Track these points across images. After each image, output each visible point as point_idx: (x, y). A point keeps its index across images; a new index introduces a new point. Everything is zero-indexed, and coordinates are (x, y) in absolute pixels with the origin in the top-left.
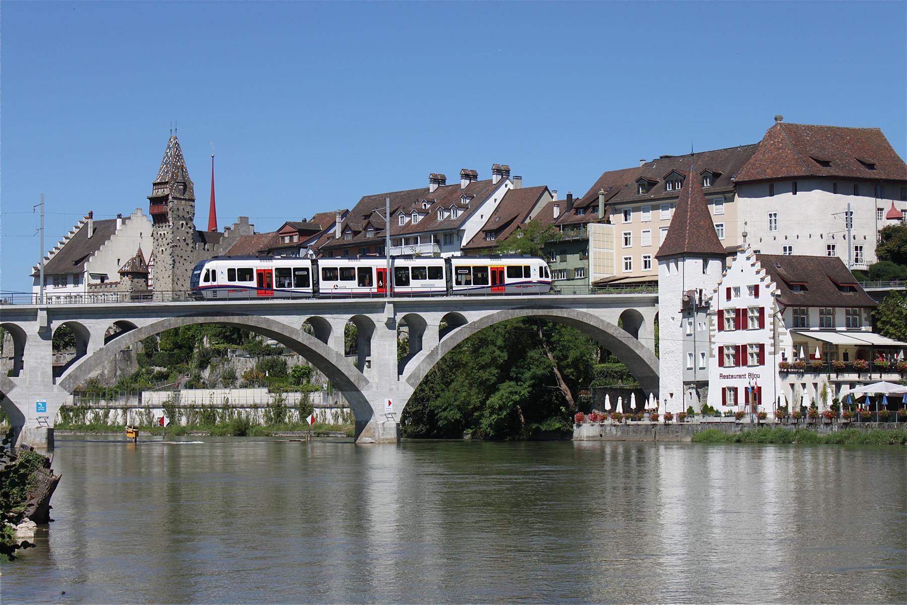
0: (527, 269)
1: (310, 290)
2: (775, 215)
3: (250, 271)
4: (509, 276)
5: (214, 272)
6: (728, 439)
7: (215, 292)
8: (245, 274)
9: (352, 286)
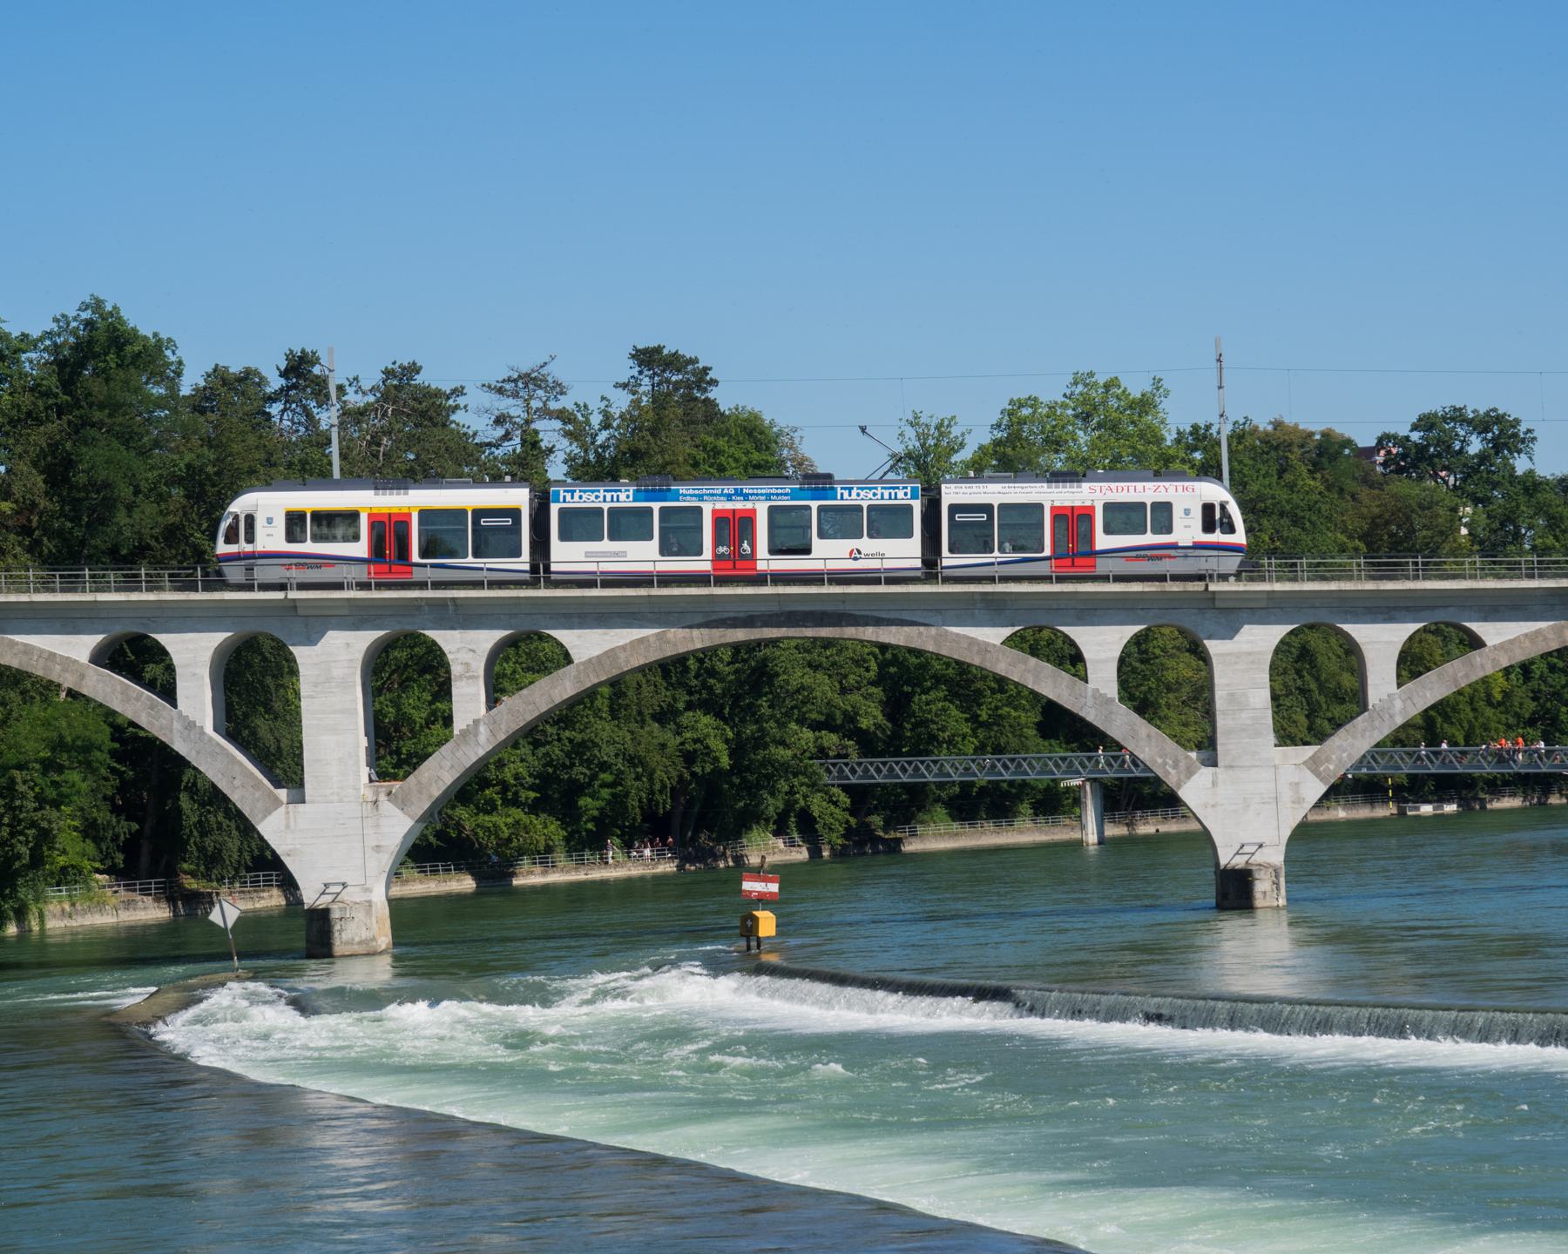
0: (1163, 511)
1: (523, 562)
2: (356, 379)
3: (352, 516)
4: (1108, 530)
5: (250, 520)
6: (1080, 1012)
7: (250, 569)
8: (330, 523)
9: (643, 555)
